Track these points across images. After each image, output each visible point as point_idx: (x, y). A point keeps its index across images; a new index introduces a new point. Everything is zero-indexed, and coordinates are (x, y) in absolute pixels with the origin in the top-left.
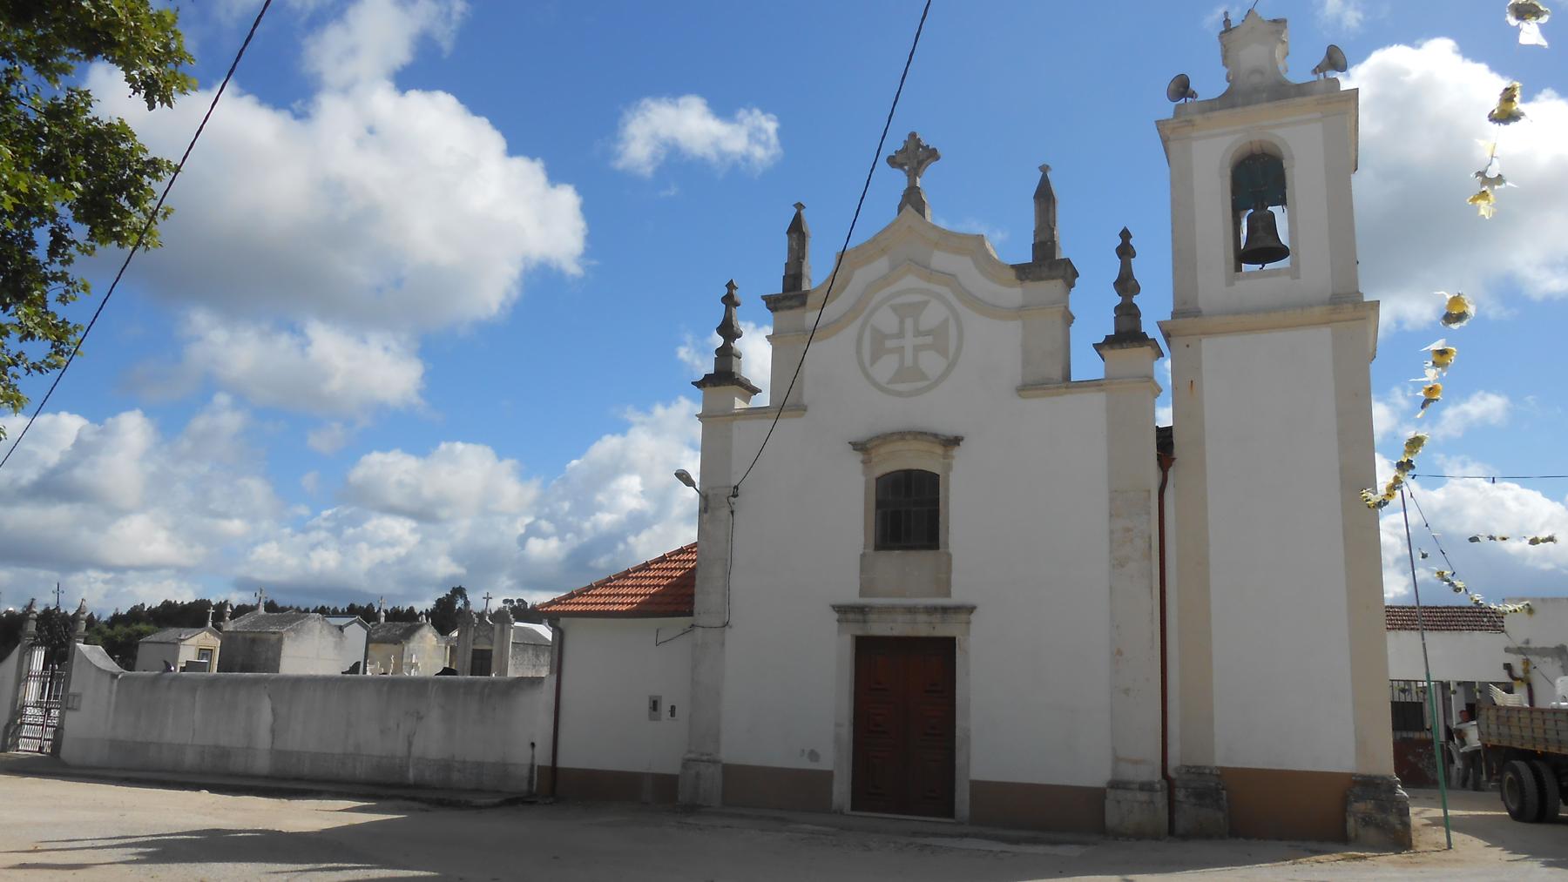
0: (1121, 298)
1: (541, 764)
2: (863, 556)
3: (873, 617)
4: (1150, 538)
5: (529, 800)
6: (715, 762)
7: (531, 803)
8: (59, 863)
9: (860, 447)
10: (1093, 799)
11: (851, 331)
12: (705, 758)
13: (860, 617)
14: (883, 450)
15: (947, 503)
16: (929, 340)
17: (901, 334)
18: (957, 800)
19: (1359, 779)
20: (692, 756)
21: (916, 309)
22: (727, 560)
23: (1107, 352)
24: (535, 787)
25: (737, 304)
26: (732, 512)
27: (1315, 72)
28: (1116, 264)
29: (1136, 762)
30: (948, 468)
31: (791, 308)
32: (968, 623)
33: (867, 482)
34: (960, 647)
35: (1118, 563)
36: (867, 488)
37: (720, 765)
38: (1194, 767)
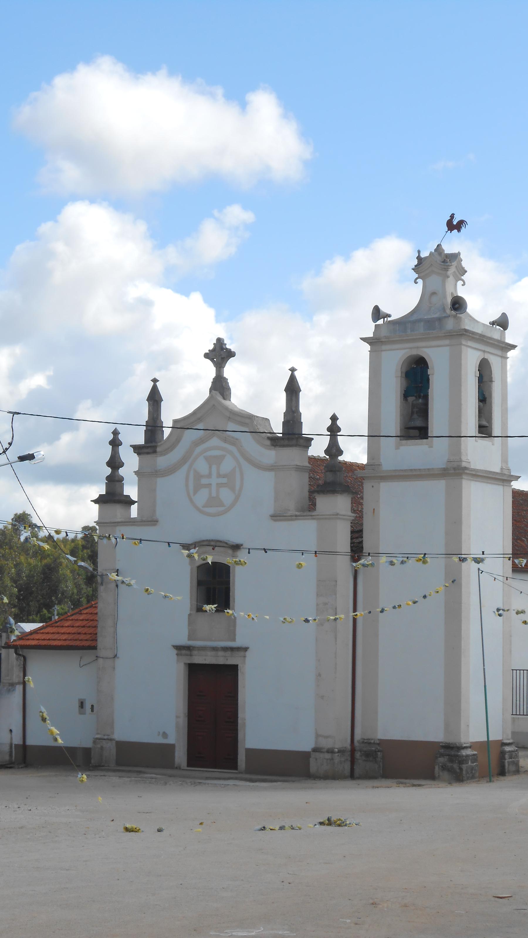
1: (16, 743)
2: (190, 615)
3: (195, 652)
5: (9, 766)
6: (111, 740)
7: (11, 768)
8: (197, 575)
10: (305, 756)
11: (182, 473)
12: (106, 737)
13: (188, 652)
15: (234, 584)
16: (225, 480)
17: (209, 476)
18: (239, 760)
21: (219, 460)
22: (115, 616)
24: (13, 758)
29: (327, 737)
31: (148, 453)
32: (245, 657)
33: (192, 569)
36: (191, 573)
37: (114, 742)
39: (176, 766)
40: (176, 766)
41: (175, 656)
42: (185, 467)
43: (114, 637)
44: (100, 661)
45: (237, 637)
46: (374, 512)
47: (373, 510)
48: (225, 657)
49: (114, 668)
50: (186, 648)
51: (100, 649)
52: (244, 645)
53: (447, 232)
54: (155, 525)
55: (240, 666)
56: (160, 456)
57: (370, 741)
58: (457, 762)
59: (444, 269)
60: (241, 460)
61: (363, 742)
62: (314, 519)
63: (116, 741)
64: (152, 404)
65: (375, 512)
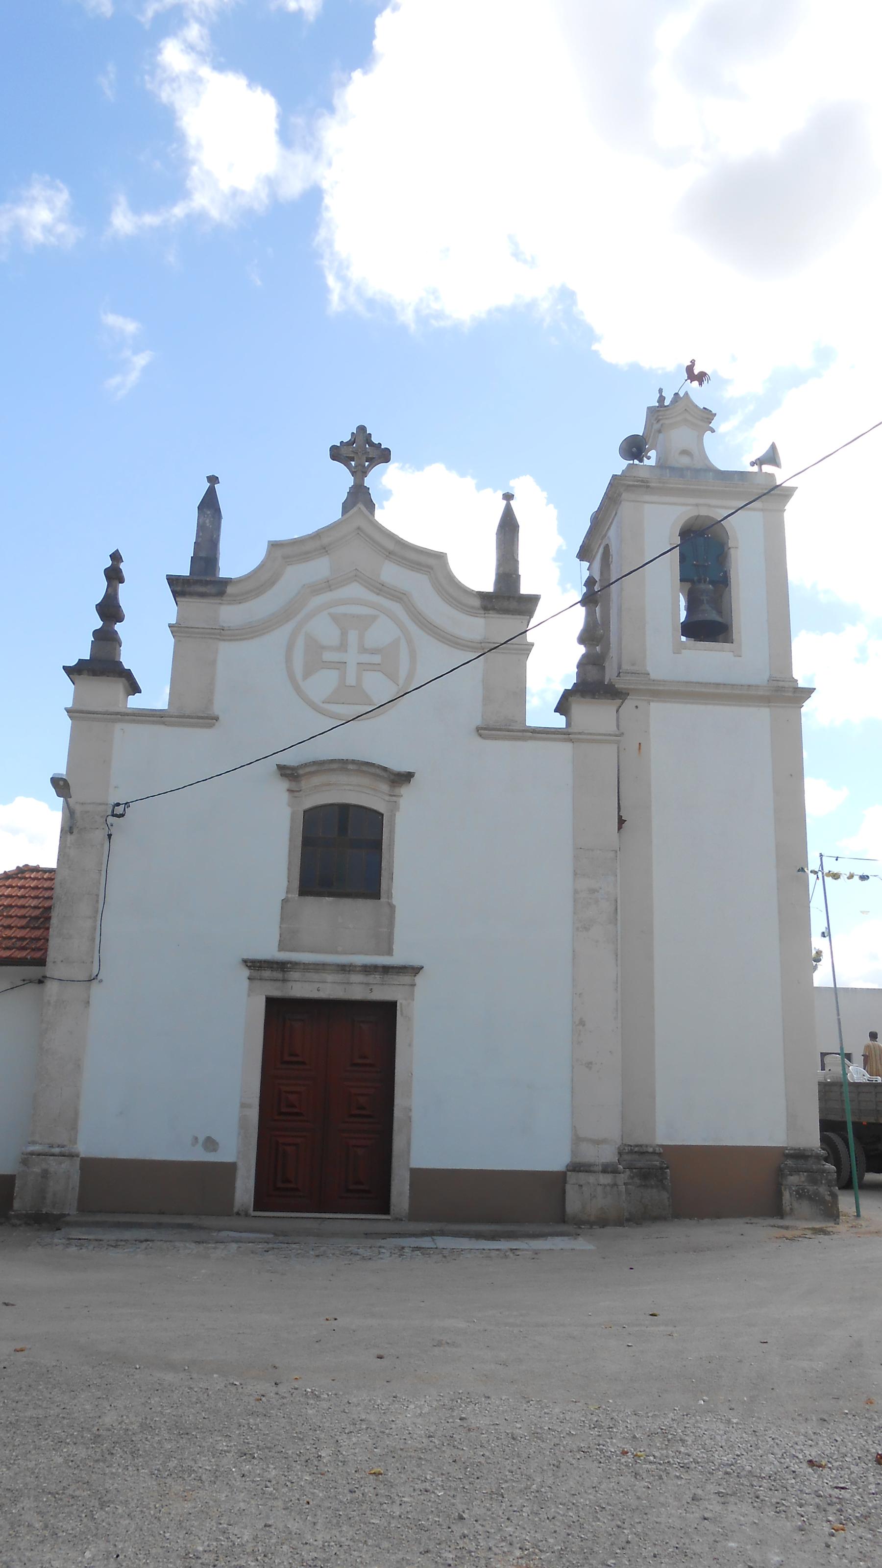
0: (102, 622)
2: (285, 901)
4: (616, 901)
6: (72, 1156)
9: (288, 773)
11: (280, 635)
12: (56, 1150)
13: (278, 975)
14: (316, 780)
17: (343, 646)
19: (792, 1152)
20: (36, 1148)
22: (98, 896)
23: (75, 677)
25: (122, 581)
26: (110, 836)
27: (753, 464)
28: (102, 585)
29: (597, 1142)
30: (394, 807)
31: (202, 595)
32: (413, 985)
34: (402, 1014)
35: (582, 926)
36: (293, 820)
38: (637, 1146)
39: (235, 1210)
40: (235, 1210)
41: (246, 982)
42: (286, 630)
43: (93, 939)
44: (52, 987)
45: (395, 947)
46: (640, 748)
47: (638, 745)
48: (367, 984)
49: (88, 1002)
50: (275, 966)
51: (54, 962)
52: (415, 962)
53: (686, 380)
54: (210, 726)
55: (401, 1004)
56: (229, 604)
57: (645, 1149)
58: (823, 1182)
59: (706, 420)
60: (413, 628)
61: (631, 1152)
62: (571, 740)
63: (84, 1161)
64: (210, 515)
65: (641, 748)
